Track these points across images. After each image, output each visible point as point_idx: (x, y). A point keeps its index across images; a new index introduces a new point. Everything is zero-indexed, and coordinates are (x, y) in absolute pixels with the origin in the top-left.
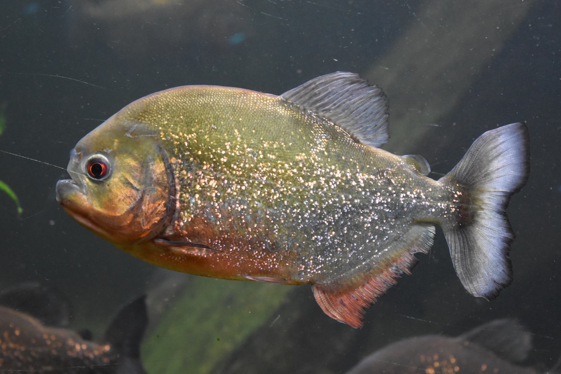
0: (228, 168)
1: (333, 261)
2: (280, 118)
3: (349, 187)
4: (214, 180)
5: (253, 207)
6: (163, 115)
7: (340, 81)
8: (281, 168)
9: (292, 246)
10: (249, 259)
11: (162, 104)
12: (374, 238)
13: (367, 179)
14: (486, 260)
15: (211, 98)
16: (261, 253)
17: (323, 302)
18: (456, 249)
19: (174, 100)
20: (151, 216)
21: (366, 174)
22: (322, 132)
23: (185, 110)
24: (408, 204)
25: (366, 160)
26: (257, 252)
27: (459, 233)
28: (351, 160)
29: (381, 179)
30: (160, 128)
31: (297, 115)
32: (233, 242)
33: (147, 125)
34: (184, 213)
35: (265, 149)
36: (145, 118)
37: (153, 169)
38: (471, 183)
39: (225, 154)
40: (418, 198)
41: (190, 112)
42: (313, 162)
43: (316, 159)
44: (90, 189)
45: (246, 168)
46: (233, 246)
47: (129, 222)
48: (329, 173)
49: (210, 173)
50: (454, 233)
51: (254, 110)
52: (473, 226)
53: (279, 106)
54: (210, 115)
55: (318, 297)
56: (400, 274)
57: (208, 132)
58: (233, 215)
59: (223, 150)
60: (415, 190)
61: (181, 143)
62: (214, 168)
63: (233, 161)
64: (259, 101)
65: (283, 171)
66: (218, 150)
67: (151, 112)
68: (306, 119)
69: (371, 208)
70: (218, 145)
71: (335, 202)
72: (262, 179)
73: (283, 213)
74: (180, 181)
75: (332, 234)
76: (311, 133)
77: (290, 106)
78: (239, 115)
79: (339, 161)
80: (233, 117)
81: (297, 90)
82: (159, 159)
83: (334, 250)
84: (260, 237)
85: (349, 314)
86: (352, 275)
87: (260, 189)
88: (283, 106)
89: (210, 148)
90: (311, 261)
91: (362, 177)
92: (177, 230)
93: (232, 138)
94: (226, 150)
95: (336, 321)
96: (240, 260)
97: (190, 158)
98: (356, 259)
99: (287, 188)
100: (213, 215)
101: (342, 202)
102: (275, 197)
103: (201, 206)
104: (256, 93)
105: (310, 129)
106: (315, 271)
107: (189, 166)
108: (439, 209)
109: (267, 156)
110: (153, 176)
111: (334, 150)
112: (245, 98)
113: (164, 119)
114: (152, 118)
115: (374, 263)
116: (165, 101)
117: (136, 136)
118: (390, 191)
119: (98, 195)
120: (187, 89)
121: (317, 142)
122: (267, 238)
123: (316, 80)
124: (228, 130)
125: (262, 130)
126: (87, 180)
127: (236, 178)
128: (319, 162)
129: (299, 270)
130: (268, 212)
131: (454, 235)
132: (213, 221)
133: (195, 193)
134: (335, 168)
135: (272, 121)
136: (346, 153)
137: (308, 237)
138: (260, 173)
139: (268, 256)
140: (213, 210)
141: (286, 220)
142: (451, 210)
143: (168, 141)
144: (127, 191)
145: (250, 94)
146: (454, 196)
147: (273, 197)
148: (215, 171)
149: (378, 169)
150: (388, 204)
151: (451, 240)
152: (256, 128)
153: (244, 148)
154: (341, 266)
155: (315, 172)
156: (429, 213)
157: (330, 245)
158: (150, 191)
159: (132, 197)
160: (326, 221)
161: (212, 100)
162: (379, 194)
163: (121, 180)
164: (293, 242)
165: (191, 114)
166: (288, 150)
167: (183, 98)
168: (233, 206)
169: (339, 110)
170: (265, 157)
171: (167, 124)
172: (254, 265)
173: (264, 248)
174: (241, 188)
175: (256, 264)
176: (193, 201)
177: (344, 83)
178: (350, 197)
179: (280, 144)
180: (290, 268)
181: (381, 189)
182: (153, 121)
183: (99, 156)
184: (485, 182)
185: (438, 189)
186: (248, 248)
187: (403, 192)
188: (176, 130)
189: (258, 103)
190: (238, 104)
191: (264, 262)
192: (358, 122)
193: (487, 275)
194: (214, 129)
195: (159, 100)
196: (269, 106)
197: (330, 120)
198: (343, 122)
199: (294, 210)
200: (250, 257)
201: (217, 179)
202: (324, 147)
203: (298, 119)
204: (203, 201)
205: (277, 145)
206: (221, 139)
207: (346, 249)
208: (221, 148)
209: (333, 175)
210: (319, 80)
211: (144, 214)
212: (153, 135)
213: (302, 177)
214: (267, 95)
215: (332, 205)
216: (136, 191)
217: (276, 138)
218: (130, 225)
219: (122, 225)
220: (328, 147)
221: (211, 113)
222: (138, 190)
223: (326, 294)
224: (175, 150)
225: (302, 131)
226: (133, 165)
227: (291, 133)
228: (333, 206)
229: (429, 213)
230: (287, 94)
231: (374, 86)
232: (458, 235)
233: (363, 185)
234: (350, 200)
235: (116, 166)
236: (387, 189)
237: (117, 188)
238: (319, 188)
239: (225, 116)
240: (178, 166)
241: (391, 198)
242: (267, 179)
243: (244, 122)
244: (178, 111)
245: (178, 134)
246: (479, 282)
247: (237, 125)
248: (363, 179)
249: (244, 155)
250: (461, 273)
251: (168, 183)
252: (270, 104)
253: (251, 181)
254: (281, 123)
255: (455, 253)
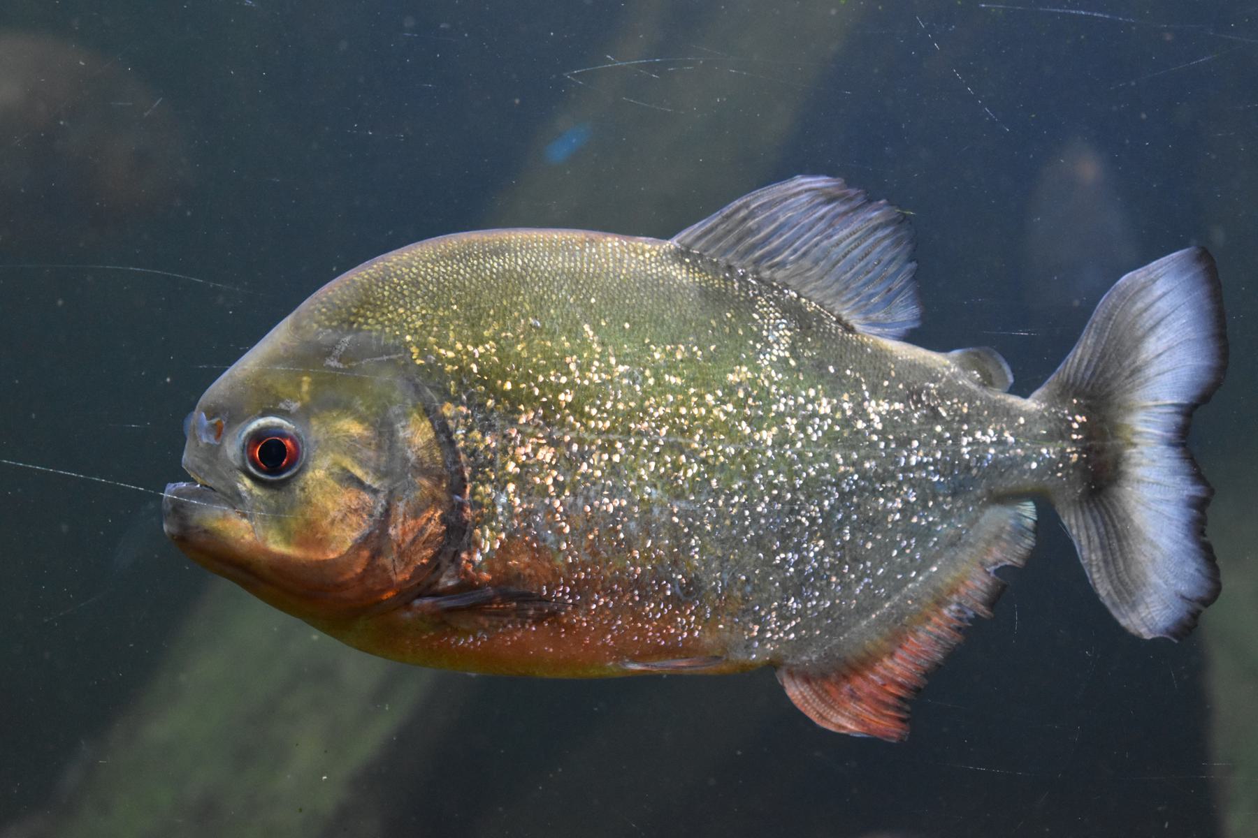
0: (577, 416)
1: (821, 608)
2: (682, 291)
3: (850, 435)
4: (546, 447)
5: (642, 500)
6: (409, 306)
7: (804, 198)
8: (698, 405)
9: (731, 583)
10: (636, 623)
11: (402, 282)
12: (909, 545)
13: (888, 412)
14: (1157, 554)
15: (516, 256)
16: (662, 607)
17: (811, 701)
18: (1092, 544)
19: (429, 270)
20: (412, 548)
21: (883, 400)
22: (777, 314)
23: (460, 291)
24: (980, 460)
25: (880, 368)
26: (653, 605)
27: (1092, 505)
28: (848, 372)
29: (917, 409)
30: (408, 338)
31: (716, 281)
32: (599, 587)
33: (374, 334)
34: (483, 532)
35: (656, 364)
36: (367, 318)
37: (405, 438)
38: (1104, 394)
39: (567, 384)
40: (1001, 442)
41: (473, 294)
42: (767, 383)
43: (773, 378)
44: (257, 504)
45: (618, 411)
46: (599, 598)
47: (359, 570)
48: (804, 407)
49: (537, 430)
50: (1081, 507)
51: (619, 276)
52: (1119, 486)
53: (673, 264)
54: (521, 297)
55: (797, 693)
56: (968, 618)
57: (522, 336)
58: (596, 523)
59: (563, 374)
60: (991, 427)
61: (461, 369)
62: (544, 418)
63: (588, 397)
64: (626, 255)
65: (703, 411)
66: (550, 375)
67: (379, 303)
68: (737, 288)
69: (900, 476)
70: (548, 365)
71: (821, 472)
72: (658, 434)
73: (709, 508)
74: (470, 457)
75: (817, 546)
76: (754, 318)
77: (696, 261)
78: (587, 291)
79: (822, 376)
80: (574, 297)
81: (709, 225)
82: (419, 414)
83: (824, 582)
84: (660, 569)
85: (874, 715)
86: (863, 634)
87: (655, 458)
88: (682, 262)
89: (531, 372)
90: (774, 614)
91: (877, 409)
92: (466, 573)
93: (579, 345)
94: (568, 373)
95: (846, 736)
96: (614, 628)
97: (487, 401)
98: (871, 596)
99: (714, 449)
100: (550, 529)
101: (838, 470)
102: (690, 473)
103: (521, 509)
104: (617, 239)
105: (750, 310)
106: (782, 635)
107: (488, 420)
108: (1046, 462)
109: (664, 379)
110: (409, 454)
111: (808, 353)
112: (594, 250)
113: (414, 316)
114: (385, 318)
115: (910, 602)
116: (408, 274)
117: (354, 364)
118: (939, 433)
119: (277, 515)
120: (455, 242)
121: (771, 339)
122: (677, 570)
123: (749, 199)
124: (568, 327)
125: (645, 322)
126: (248, 482)
127: (598, 438)
128: (779, 384)
129: (747, 637)
130: (676, 510)
131: (1083, 513)
132: (552, 543)
133: (507, 482)
134: (817, 393)
135: (664, 300)
136: (836, 356)
137: (767, 558)
138: (653, 421)
139: (677, 612)
140: (549, 517)
141: (718, 523)
142: (1070, 459)
143: (430, 365)
144: (349, 498)
145: (604, 240)
146: (1071, 428)
147: (685, 473)
148: (548, 425)
149: (907, 386)
150: (937, 464)
151: (1077, 525)
152: (631, 318)
153: (609, 366)
154: (839, 617)
155: (774, 407)
156: (1025, 472)
157: (815, 573)
158: (404, 491)
159: (364, 509)
160: (805, 516)
161: (520, 262)
162: (915, 443)
163: (331, 474)
164: (733, 574)
165: (477, 299)
166: (710, 361)
167: (450, 262)
168: (596, 503)
169: (806, 263)
170: (659, 382)
171: (423, 327)
172: (646, 637)
173: (669, 593)
174: (610, 459)
175: (650, 634)
176: (503, 500)
177: (813, 201)
178: (855, 456)
179: (688, 349)
180: (728, 634)
181: (919, 431)
182: (386, 323)
183: (262, 422)
184: (1133, 388)
185: (1037, 417)
186: (632, 599)
187: (967, 433)
188: (447, 337)
189: (626, 261)
190: (582, 265)
191: (669, 627)
192: (849, 285)
193: (1165, 587)
194: (536, 327)
195: (392, 274)
196: (650, 265)
197: (787, 287)
198: (815, 289)
199: (732, 498)
200: (638, 617)
201: (552, 443)
202: (786, 349)
203: (719, 290)
204: (526, 497)
205: (683, 353)
206: (555, 350)
207: (849, 578)
208: (557, 371)
209: (814, 410)
210: (757, 198)
211: (395, 547)
212: (394, 357)
213: (746, 419)
214: (641, 241)
215: (816, 479)
216: (372, 495)
217: (679, 338)
218: (361, 578)
219: (341, 579)
220: (795, 348)
221: (522, 292)
222: (375, 492)
223: (813, 684)
224: (451, 386)
225: (733, 316)
226: (358, 434)
227: (710, 323)
228: (818, 481)
229: (1025, 472)
230: (687, 235)
231: (882, 202)
232: (1091, 510)
233: (879, 426)
234: (853, 464)
235: (317, 442)
236: (932, 429)
237: (325, 494)
238: (786, 442)
239: (557, 295)
240: (462, 421)
241: (942, 451)
242: (668, 432)
243: (602, 307)
244: (443, 293)
245: (452, 348)
246: (1150, 606)
247: (588, 313)
248: (879, 414)
249: (611, 381)
250: (1108, 594)
251: (445, 466)
252: (653, 259)
253: (632, 441)
254: (685, 301)
255: (1091, 552)
